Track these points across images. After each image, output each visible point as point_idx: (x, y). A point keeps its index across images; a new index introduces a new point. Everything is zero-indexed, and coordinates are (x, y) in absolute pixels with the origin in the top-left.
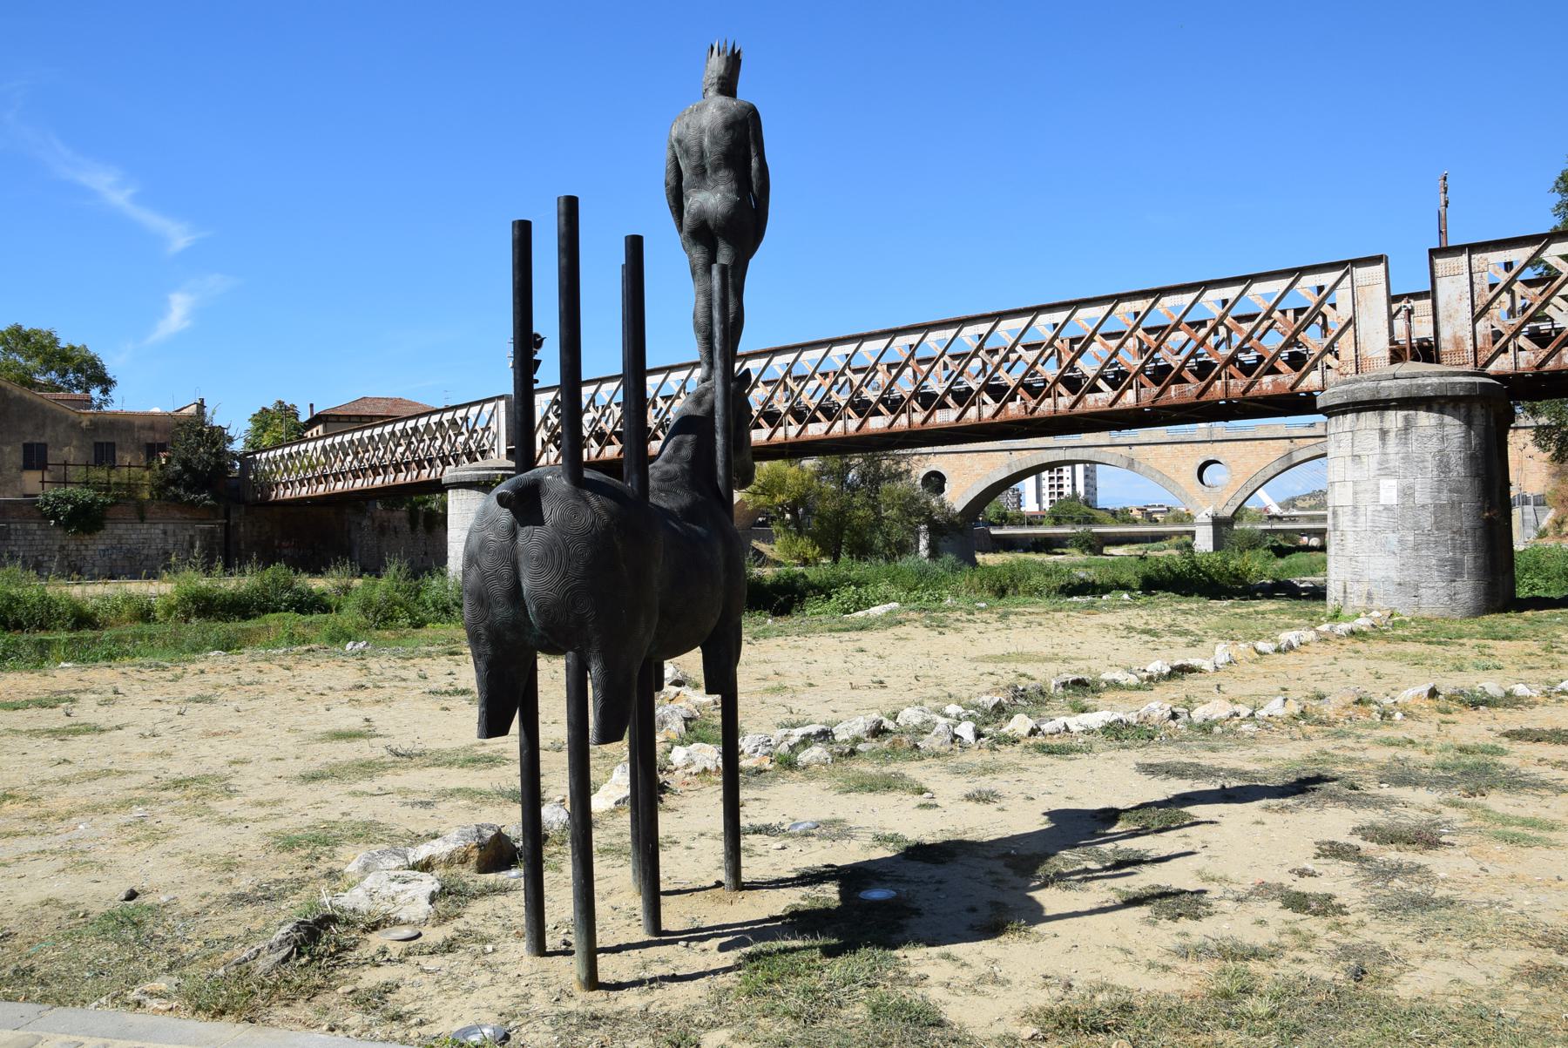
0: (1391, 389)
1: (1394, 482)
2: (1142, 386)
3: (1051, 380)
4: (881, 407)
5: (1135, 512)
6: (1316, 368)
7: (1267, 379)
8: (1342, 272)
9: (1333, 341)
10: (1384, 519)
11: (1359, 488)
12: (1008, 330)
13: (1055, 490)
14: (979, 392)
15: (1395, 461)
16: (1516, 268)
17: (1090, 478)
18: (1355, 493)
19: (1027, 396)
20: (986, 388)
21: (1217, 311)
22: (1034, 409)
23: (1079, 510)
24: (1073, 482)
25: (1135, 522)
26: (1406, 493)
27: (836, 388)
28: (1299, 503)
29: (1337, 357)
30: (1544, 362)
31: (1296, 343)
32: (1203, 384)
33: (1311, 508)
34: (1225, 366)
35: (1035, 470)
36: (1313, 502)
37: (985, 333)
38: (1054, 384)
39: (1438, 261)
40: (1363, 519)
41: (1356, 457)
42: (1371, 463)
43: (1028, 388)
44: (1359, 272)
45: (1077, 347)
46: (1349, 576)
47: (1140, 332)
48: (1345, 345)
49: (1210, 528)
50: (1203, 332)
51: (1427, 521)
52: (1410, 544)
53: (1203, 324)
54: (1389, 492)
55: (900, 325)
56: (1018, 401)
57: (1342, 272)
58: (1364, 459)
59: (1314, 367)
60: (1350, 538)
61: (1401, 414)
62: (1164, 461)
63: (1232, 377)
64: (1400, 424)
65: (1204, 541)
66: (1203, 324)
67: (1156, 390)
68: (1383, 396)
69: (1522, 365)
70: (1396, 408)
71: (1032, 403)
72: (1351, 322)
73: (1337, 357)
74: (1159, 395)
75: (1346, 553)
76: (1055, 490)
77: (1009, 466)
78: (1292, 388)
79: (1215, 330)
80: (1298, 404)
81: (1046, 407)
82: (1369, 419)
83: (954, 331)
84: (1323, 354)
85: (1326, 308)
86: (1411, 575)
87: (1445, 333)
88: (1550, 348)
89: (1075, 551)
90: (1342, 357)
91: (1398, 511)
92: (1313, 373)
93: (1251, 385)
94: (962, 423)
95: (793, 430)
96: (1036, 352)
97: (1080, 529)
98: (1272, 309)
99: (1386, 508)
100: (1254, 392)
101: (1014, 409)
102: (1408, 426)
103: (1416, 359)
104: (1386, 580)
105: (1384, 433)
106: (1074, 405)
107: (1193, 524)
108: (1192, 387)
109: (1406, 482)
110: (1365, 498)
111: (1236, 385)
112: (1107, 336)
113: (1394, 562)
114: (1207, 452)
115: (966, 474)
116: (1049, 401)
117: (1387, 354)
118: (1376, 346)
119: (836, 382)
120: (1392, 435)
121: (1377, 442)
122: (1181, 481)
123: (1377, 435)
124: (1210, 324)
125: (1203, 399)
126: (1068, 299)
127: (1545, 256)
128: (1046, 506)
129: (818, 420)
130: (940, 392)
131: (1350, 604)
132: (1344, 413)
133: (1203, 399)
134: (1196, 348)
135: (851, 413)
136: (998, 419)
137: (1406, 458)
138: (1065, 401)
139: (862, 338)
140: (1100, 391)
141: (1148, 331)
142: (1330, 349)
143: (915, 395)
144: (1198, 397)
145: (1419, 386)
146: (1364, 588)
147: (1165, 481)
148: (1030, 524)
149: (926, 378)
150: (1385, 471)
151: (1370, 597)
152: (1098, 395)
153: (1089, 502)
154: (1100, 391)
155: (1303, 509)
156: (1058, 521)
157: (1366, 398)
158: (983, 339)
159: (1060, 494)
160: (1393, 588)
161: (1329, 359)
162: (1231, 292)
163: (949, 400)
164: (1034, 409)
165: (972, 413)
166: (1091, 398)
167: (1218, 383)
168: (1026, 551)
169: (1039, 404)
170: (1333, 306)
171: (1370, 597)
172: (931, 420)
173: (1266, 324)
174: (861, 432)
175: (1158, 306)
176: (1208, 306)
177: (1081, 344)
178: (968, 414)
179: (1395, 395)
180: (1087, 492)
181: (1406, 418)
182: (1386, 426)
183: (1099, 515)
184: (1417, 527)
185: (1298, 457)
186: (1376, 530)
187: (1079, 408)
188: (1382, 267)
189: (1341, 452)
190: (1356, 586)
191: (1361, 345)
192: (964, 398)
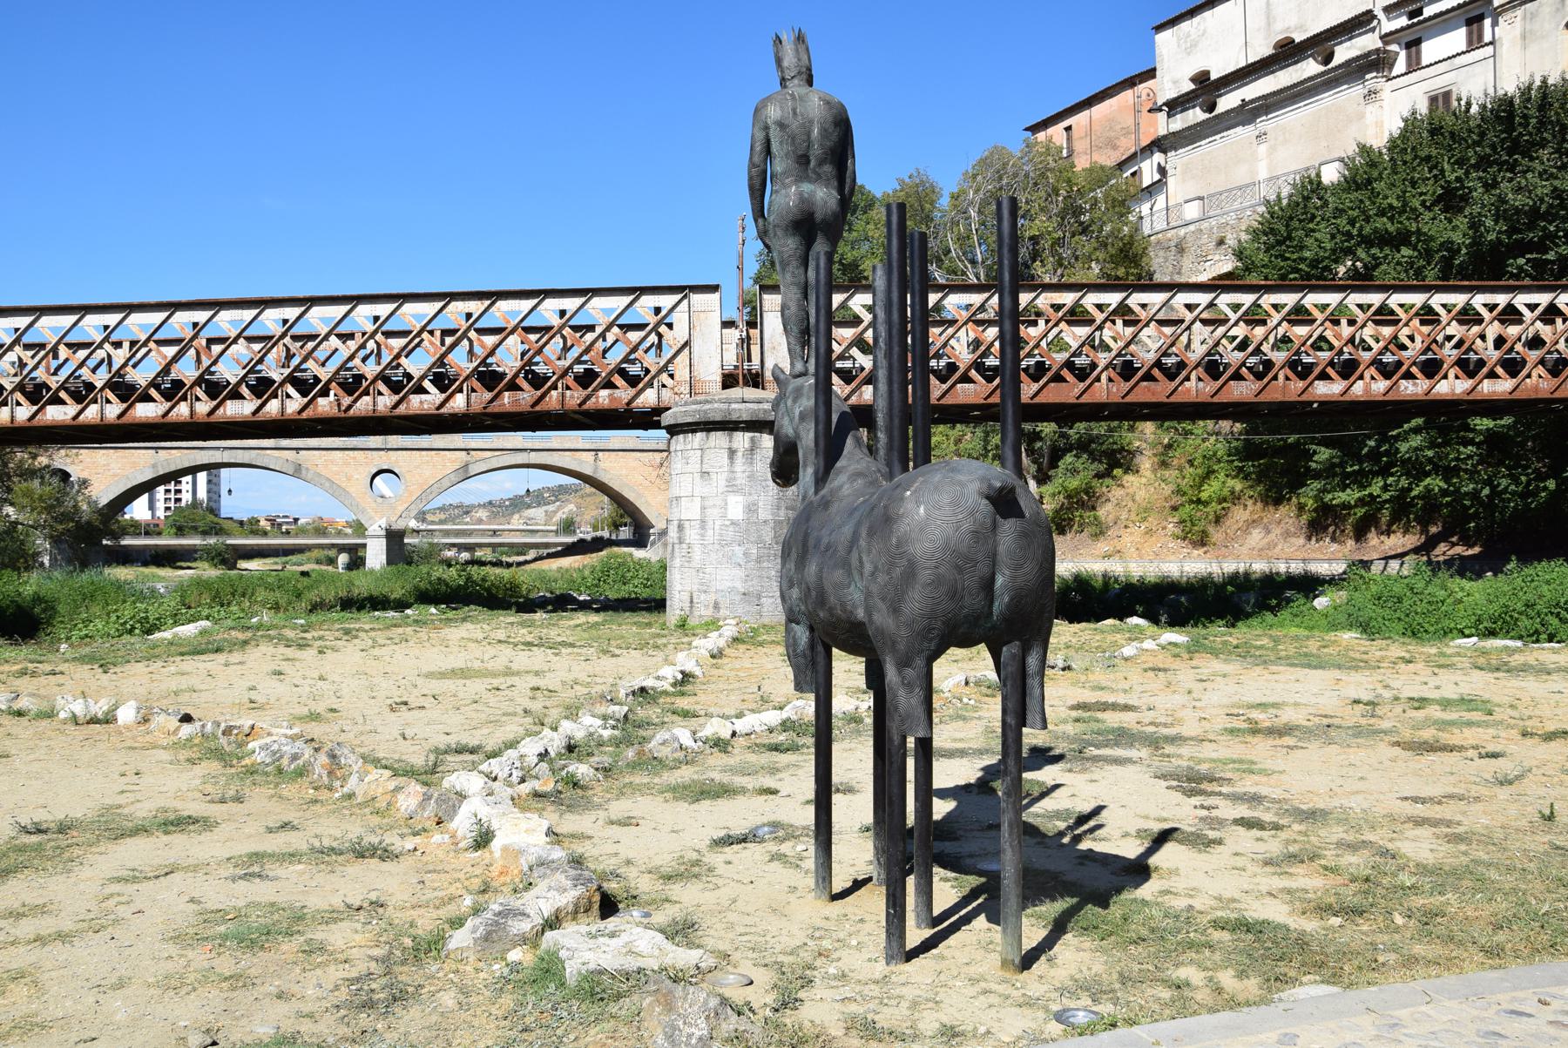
0: (715, 411)
1: (740, 498)
2: (473, 390)
3: (370, 377)
4: (153, 392)
5: (263, 523)
6: (461, 391)
7: (604, 393)
8: (679, 296)
9: (670, 361)
10: (730, 533)
11: (707, 503)
12: (320, 318)
13: (172, 496)
14: (282, 384)
15: (741, 479)
16: (663, 313)
17: (213, 485)
18: (703, 508)
19: (341, 392)
20: (292, 379)
21: (278, 330)
22: (349, 407)
23: (204, 519)
24: (194, 489)
25: (265, 534)
26: (751, 509)
27: (362, 353)
28: (429, 517)
29: (672, 376)
30: (584, 402)
31: (443, 365)
32: (539, 393)
33: (441, 522)
34: (1196, 367)
35: (193, 470)
36: (443, 516)
37: (113, 324)
38: (374, 381)
39: (765, 296)
40: (710, 532)
41: (705, 474)
42: (720, 480)
43: (387, 380)
44: (696, 298)
45: (449, 340)
46: (695, 587)
47: (287, 340)
48: (680, 367)
49: (384, 541)
50: (590, 337)
51: (768, 535)
52: (754, 557)
53: (591, 328)
54: (736, 508)
55: (136, 300)
56: (332, 397)
57: (679, 296)
58: (714, 476)
59: (650, 385)
60: (697, 554)
61: (748, 435)
62: (335, 469)
63: (568, 388)
64: (747, 445)
65: (376, 556)
66: (591, 328)
67: (488, 396)
68: (734, 417)
69: (380, 407)
70: (743, 430)
71: (347, 401)
72: (687, 344)
73: (672, 376)
74: (491, 401)
75: (693, 564)
76: (172, 496)
77: (154, 466)
78: (628, 404)
79: (603, 336)
80: (648, 419)
81: (364, 406)
82: (719, 439)
83: (254, 312)
84: (660, 372)
85: (663, 329)
86: (754, 585)
87: (769, 365)
88: (853, 385)
89: (206, 565)
90: (677, 377)
91: (743, 526)
92: (649, 391)
93: (588, 397)
94: (260, 417)
95: (203, 408)
96: (402, 342)
97: (212, 541)
98: (148, 340)
99: (733, 523)
100: (590, 404)
101: (325, 406)
102: (753, 448)
103: (746, 384)
104: (732, 590)
105: (732, 453)
106: (395, 406)
107: (365, 537)
108: (527, 395)
109: (751, 499)
110: (713, 513)
111: (572, 397)
112: (250, 339)
113: (740, 573)
114: (383, 460)
115: (102, 473)
116: (366, 399)
117: (719, 379)
118: (710, 374)
119: (363, 346)
120: (740, 454)
121: (726, 461)
122: (351, 490)
123: (726, 455)
124: (599, 330)
125: (538, 408)
126: (301, 295)
127: (851, 303)
128: (161, 513)
129: (63, 402)
130: (233, 380)
131: (697, 613)
132: (694, 431)
133: (538, 408)
134: (533, 356)
135: (111, 396)
136: (304, 415)
137: (751, 477)
138: (386, 401)
139: (130, 308)
140: (426, 392)
141: (295, 338)
142: (664, 369)
143: (199, 382)
144: (533, 406)
145: (705, 412)
146: (711, 598)
147: (335, 490)
148: (147, 533)
149: (215, 363)
150: (732, 487)
151: (716, 606)
152: (424, 397)
153: (213, 510)
154: (426, 392)
155: (433, 523)
156: (180, 531)
157: (718, 418)
158: (19, 334)
159: (178, 500)
160: (738, 598)
161: (664, 377)
162: (291, 313)
163: (244, 390)
164: (349, 407)
165: (273, 407)
166: (415, 400)
167: (554, 393)
168: (145, 564)
169: (355, 401)
170: (670, 326)
171: (716, 606)
172: (220, 411)
173: (144, 350)
174: (124, 420)
175: (493, 309)
176: (547, 315)
177: (412, 339)
178: (268, 408)
179: (745, 417)
180: (209, 499)
181: (752, 439)
182: (735, 446)
183: (227, 525)
184: (760, 540)
185: (474, 469)
186: (723, 544)
187: (402, 410)
188: (716, 296)
189: (689, 468)
190: (703, 596)
191: (695, 368)
192: (174, 392)
